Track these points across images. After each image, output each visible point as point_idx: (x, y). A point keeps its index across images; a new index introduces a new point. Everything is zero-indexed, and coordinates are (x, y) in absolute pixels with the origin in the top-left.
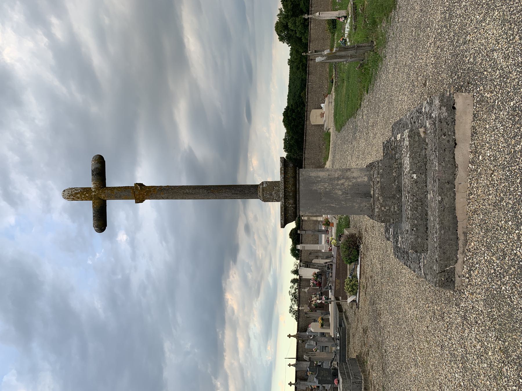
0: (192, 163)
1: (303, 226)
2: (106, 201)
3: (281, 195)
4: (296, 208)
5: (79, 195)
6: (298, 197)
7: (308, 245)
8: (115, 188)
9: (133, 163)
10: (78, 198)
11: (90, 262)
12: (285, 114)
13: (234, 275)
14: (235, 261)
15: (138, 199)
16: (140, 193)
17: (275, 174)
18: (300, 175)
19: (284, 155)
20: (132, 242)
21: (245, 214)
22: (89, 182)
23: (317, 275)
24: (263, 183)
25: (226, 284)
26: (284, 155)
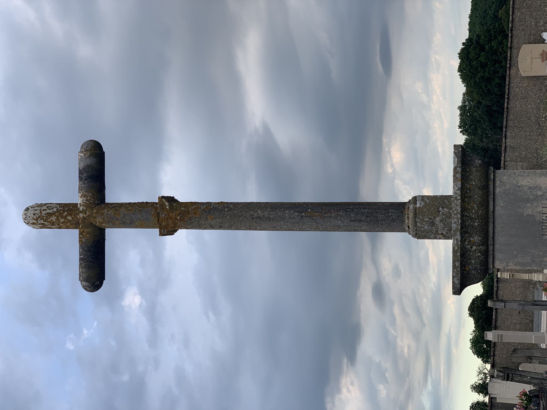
0: (269, 158)
1: (500, 292)
2: (104, 230)
3: (455, 223)
4: (486, 254)
5: (54, 218)
6: (491, 229)
7: (510, 333)
8: (122, 204)
9: (157, 155)
10: (53, 224)
11: (70, 346)
12: (464, 55)
13: (351, 387)
14: (352, 358)
15: (166, 227)
16: (169, 216)
17: (442, 181)
18: (498, 183)
19: (461, 139)
20: (152, 312)
21: (375, 261)
22: (71, 192)
23: (529, 398)
24: (415, 199)
25: (333, 403)
26: (461, 139)
